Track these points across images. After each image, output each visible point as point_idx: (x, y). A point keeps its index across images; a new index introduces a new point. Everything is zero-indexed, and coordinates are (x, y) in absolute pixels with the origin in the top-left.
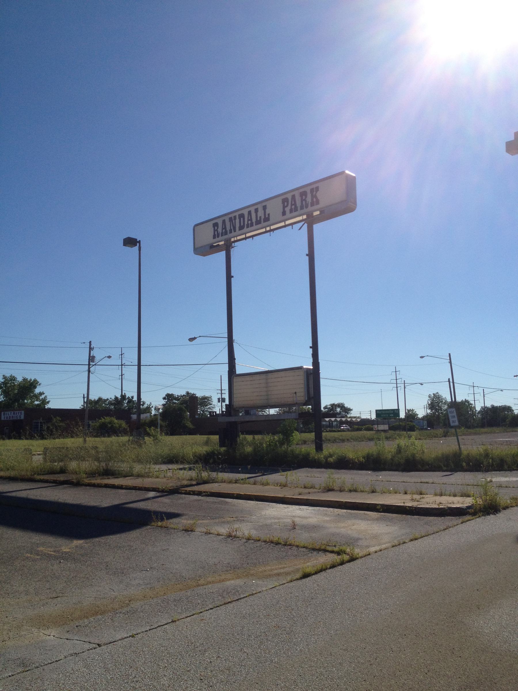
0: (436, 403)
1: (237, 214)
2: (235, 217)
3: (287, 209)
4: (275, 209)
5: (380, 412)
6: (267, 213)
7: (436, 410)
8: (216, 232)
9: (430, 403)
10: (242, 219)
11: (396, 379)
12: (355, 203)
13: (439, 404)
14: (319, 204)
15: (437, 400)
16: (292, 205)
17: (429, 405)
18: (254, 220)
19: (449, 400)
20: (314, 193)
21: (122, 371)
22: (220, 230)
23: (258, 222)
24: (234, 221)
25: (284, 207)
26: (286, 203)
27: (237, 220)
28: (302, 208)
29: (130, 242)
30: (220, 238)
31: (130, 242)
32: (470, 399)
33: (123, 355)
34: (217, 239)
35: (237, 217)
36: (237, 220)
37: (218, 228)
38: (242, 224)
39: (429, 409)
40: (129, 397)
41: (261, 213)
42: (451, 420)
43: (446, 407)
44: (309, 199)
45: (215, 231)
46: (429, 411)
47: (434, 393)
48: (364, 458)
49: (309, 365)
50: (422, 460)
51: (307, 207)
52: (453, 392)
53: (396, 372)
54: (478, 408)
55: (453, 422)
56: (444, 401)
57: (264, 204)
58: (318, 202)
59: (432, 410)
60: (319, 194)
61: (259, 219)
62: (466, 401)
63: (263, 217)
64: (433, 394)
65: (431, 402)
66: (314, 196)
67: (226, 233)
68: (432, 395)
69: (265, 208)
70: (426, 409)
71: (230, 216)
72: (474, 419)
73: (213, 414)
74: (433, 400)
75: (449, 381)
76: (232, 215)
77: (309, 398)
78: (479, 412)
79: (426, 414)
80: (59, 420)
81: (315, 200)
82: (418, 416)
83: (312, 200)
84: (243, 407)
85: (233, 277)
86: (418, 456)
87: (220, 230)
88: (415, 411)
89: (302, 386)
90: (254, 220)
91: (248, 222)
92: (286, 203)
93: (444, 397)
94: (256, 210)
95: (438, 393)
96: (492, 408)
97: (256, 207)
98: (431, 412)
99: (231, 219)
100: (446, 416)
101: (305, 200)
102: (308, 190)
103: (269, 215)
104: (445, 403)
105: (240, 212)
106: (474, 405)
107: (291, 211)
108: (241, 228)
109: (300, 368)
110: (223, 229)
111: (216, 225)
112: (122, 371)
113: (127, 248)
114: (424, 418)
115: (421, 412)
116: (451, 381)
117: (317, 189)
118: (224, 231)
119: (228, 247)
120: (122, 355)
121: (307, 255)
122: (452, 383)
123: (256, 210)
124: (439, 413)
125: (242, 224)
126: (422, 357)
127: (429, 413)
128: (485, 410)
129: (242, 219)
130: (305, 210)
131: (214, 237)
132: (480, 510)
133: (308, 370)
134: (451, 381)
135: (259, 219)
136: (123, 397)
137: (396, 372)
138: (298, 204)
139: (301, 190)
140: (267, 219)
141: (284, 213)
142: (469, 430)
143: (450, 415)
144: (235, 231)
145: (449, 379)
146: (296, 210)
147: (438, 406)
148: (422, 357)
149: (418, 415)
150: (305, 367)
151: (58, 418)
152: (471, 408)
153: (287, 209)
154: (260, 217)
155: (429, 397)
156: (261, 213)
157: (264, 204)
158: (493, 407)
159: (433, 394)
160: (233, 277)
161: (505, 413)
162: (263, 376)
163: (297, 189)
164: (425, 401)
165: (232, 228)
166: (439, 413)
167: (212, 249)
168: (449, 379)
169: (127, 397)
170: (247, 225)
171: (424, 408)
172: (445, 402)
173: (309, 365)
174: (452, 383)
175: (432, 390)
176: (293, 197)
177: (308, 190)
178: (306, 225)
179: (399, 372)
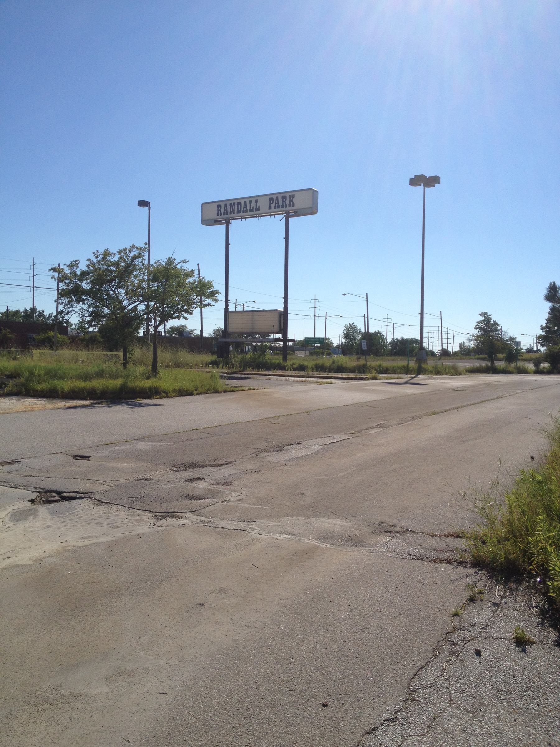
0: (351, 332)
1: (236, 202)
2: (234, 203)
3: (273, 206)
4: (264, 205)
5: (308, 340)
6: (258, 205)
7: (351, 339)
8: (219, 211)
9: (345, 332)
10: (239, 206)
11: (315, 308)
12: (317, 209)
13: (354, 334)
14: (289, 195)
15: (352, 330)
16: (276, 203)
17: (344, 334)
18: (248, 208)
19: (363, 331)
20: (292, 198)
21: (33, 283)
22: (222, 210)
23: (251, 210)
24: (233, 206)
25: (270, 204)
26: (272, 202)
27: (236, 206)
28: (283, 207)
29: (143, 204)
30: (222, 216)
31: (143, 204)
32: (383, 331)
33: (35, 266)
34: (220, 217)
35: (236, 204)
36: (236, 206)
37: (221, 209)
38: (239, 210)
39: (344, 338)
40: (39, 311)
41: (253, 204)
42: (363, 346)
43: (360, 337)
44: (288, 202)
45: (218, 210)
46: (344, 340)
47: (351, 323)
48: (314, 365)
49: (281, 309)
50: (346, 367)
51: (286, 206)
52: (367, 325)
53: (315, 300)
54: (389, 340)
55: (364, 347)
56: (358, 332)
57: (256, 199)
58: (293, 205)
59: (347, 339)
60: (294, 200)
61: (252, 208)
62: (379, 332)
63: (255, 208)
64: (349, 324)
65: (346, 332)
66: (291, 201)
67: (227, 214)
68: (348, 325)
69: (256, 201)
70: (341, 338)
71: (230, 202)
72: (384, 350)
73: (159, 334)
74: (348, 330)
75: (364, 316)
76: (233, 202)
77: (281, 329)
78: (390, 343)
79: (341, 343)
80: (9, 332)
81: (291, 203)
82: (334, 345)
83: (290, 202)
84: (237, 333)
85: (230, 244)
86: (344, 365)
87: (222, 210)
88: (331, 339)
89: (277, 322)
90: (248, 208)
91: (244, 209)
92: (272, 202)
93: (359, 327)
94: (250, 202)
95: (353, 323)
96: (402, 340)
97: (250, 199)
98: (346, 341)
99: (231, 204)
100: (360, 345)
101: (285, 202)
102: (287, 195)
103: (259, 206)
104: (359, 333)
105: (239, 201)
106: (386, 337)
107: (275, 207)
108: (239, 212)
109: (276, 310)
110: (224, 210)
111: (219, 206)
112: (33, 283)
113: (141, 208)
114: (338, 347)
115: (337, 339)
116: (366, 316)
117: (294, 196)
118: (225, 211)
119: (228, 224)
120: (33, 265)
121: (284, 238)
122: (366, 318)
123: (250, 202)
124: (353, 343)
125: (239, 210)
126: (344, 295)
127: (344, 342)
128: (395, 343)
129: (239, 206)
130: (284, 209)
131: (218, 215)
132: (370, 378)
133: (281, 311)
134: (366, 316)
135: (252, 208)
136: (34, 309)
137: (315, 300)
138: (280, 203)
139: (283, 195)
140: (258, 209)
141: (270, 208)
142: (377, 357)
143: (363, 343)
144: (234, 213)
145: (365, 315)
146: (278, 207)
147: (353, 336)
148: (344, 295)
149: (333, 343)
150: (278, 310)
151: (8, 330)
152: (383, 339)
153: (273, 206)
154: (253, 207)
155: (345, 326)
156: (253, 204)
157: (256, 199)
158: (403, 339)
159: (349, 324)
160: (230, 244)
161: (413, 346)
162: (251, 314)
163: (280, 193)
164: (341, 331)
165: (232, 210)
166: (353, 343)
167: (217, 222)
168: (365, 315)
169: (38, 311)
170: (243, 211)
171: (339, 337)
172: (359, 333)
173: (281, 309)
174: (366, 318)
175: (348, 322)
176: (277, 198)
177: (287, 195)
178: (285, 218)
179: (318, 300)
